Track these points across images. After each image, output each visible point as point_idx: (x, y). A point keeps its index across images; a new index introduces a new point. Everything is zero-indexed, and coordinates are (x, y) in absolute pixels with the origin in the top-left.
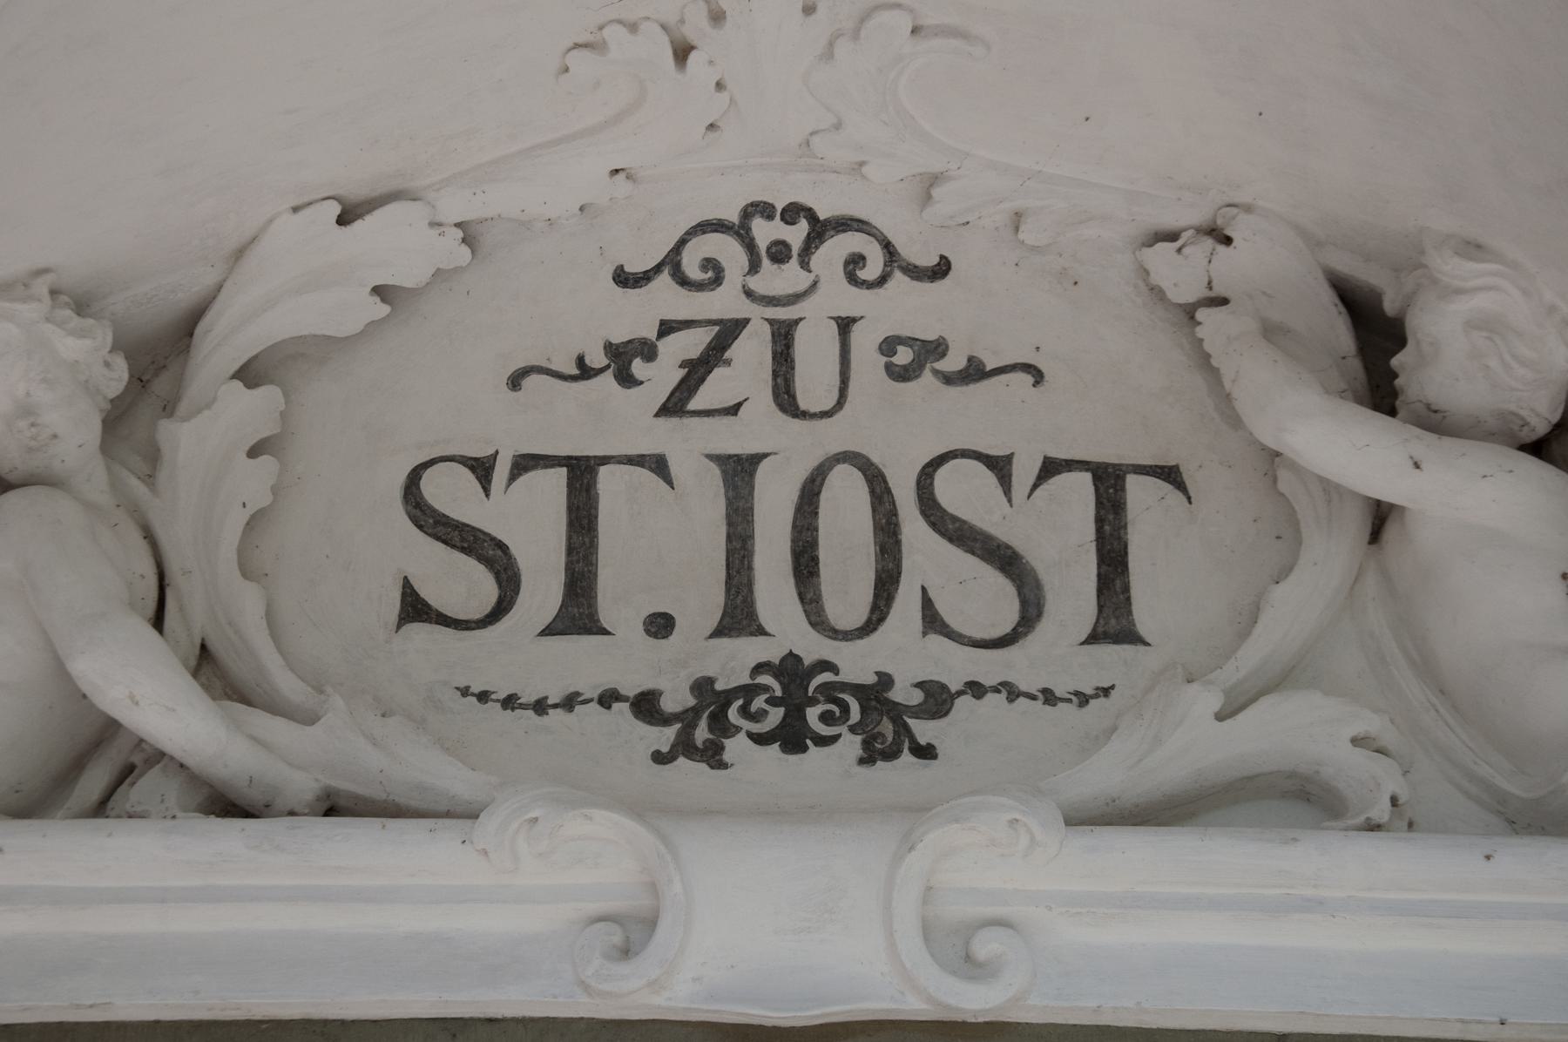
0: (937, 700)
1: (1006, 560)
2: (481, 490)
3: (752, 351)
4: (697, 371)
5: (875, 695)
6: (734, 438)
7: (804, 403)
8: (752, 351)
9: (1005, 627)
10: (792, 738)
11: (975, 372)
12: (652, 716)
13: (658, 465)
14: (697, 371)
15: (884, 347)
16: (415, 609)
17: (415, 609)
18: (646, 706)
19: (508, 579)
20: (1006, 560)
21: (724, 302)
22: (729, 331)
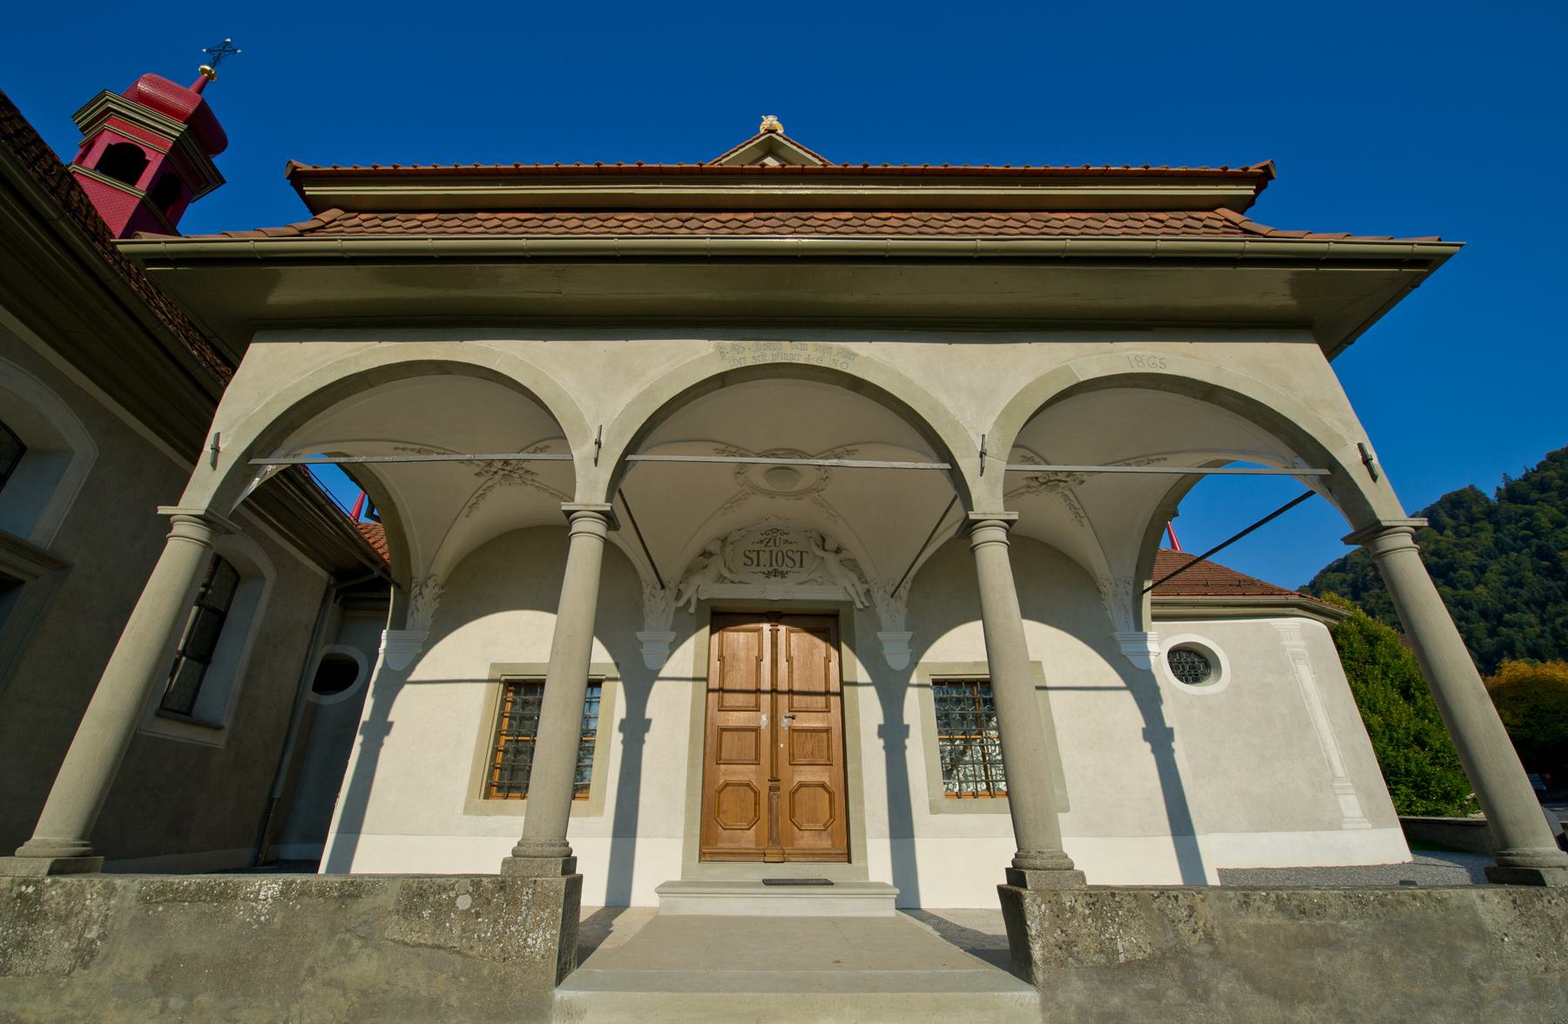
0: (787, 572)
1: (793, 560)
2: (1200, 483)
3: (772, 541)
4: (768, 543)
5: (782, 572)
6: (771, 549)
7: (826, 548)
8: (772, 541)
9: (802, 789)
10: (775, 576)
11: (791, 543)
12: (473, 883)
13: (764, 551)
14: (768, 543)
15: (1475, 878)
16: (745, 564)
17: (745, 564)
18: (764, 573)
19: (752, 561)
20: (793, 560)
21: (769, 537)
22: (770, 539)
